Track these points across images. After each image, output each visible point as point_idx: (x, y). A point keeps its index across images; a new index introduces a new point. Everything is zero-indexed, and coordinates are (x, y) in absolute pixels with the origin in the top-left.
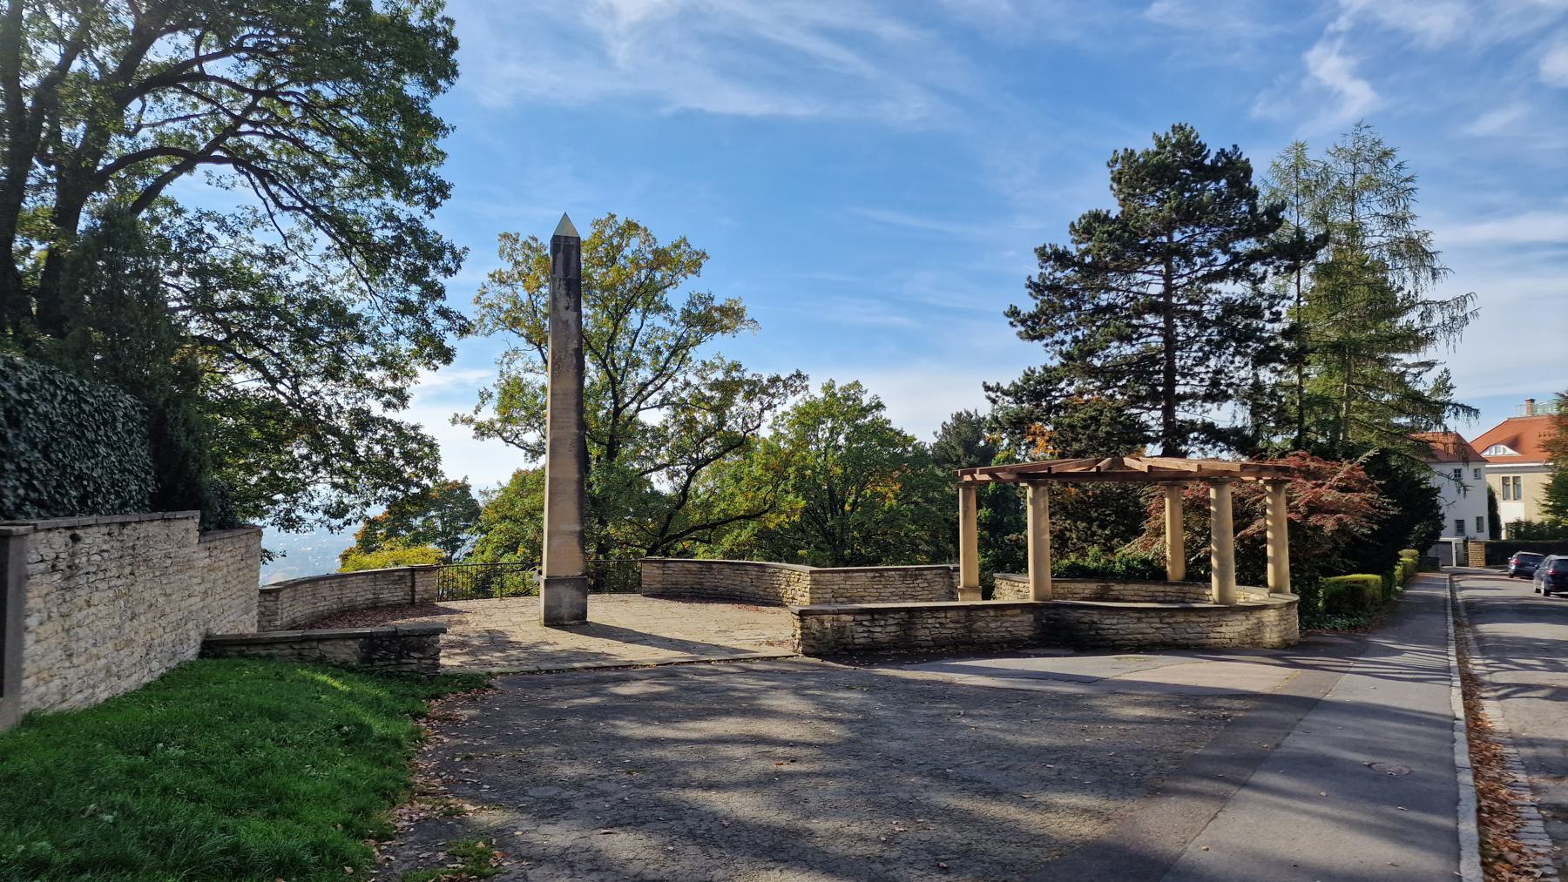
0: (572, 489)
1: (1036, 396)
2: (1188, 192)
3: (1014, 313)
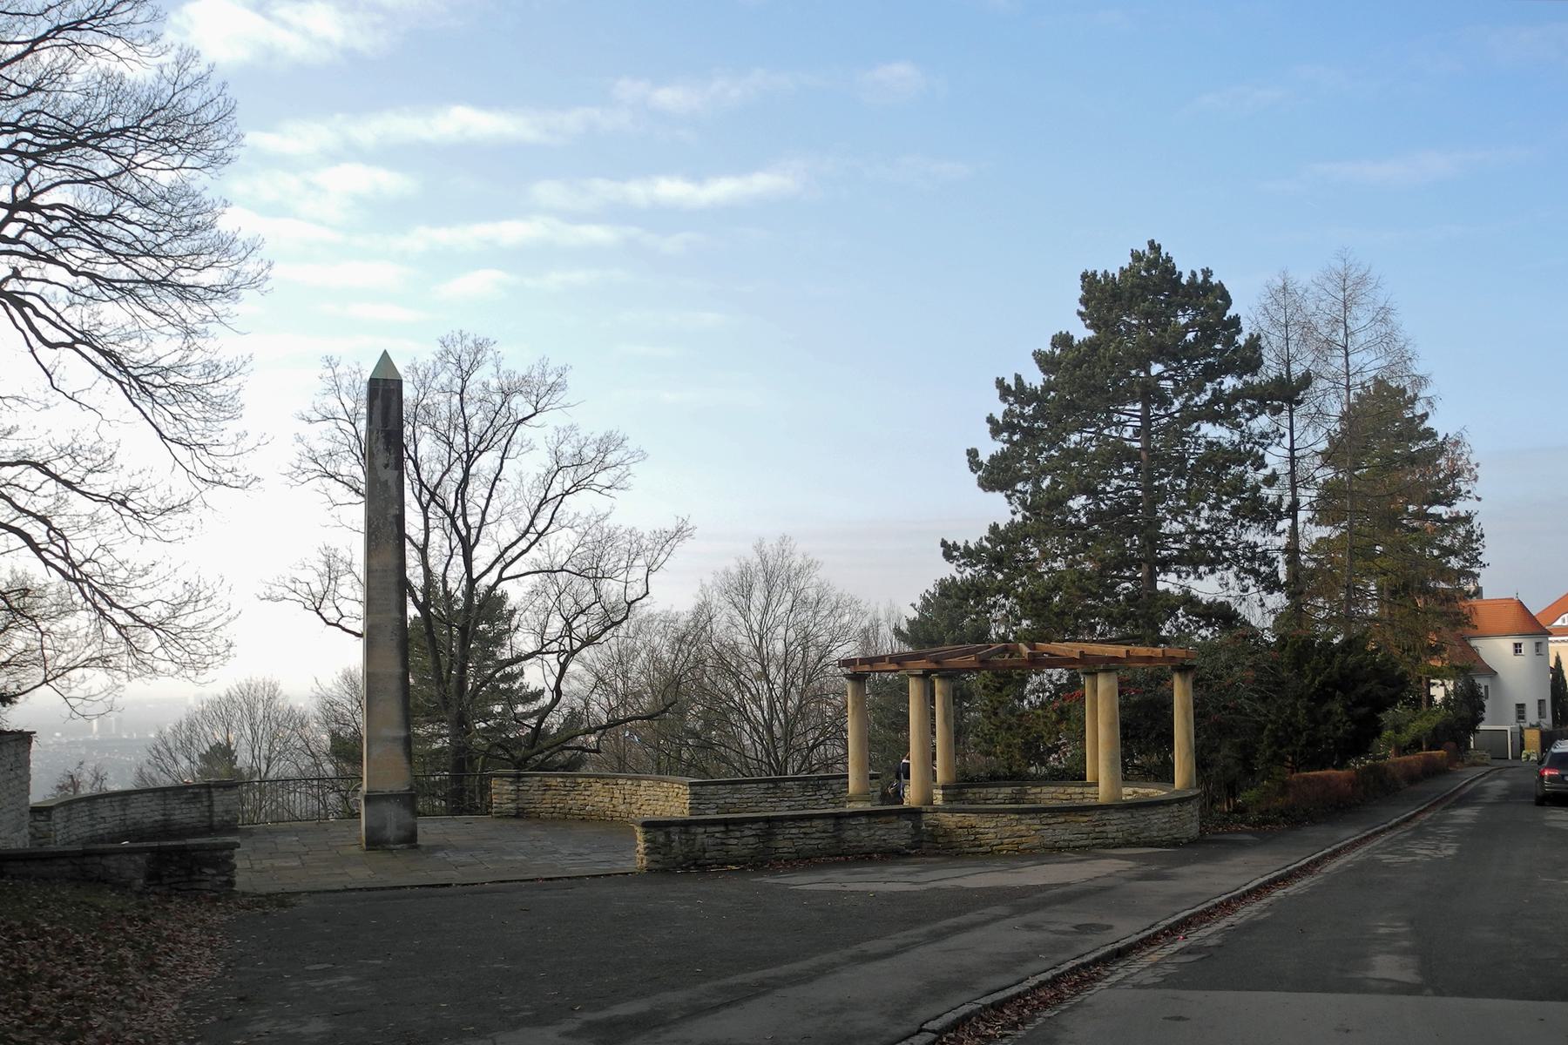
0: (394, 685)
1: (998, 561)
2: (1152, 323)
3: (973, 454)
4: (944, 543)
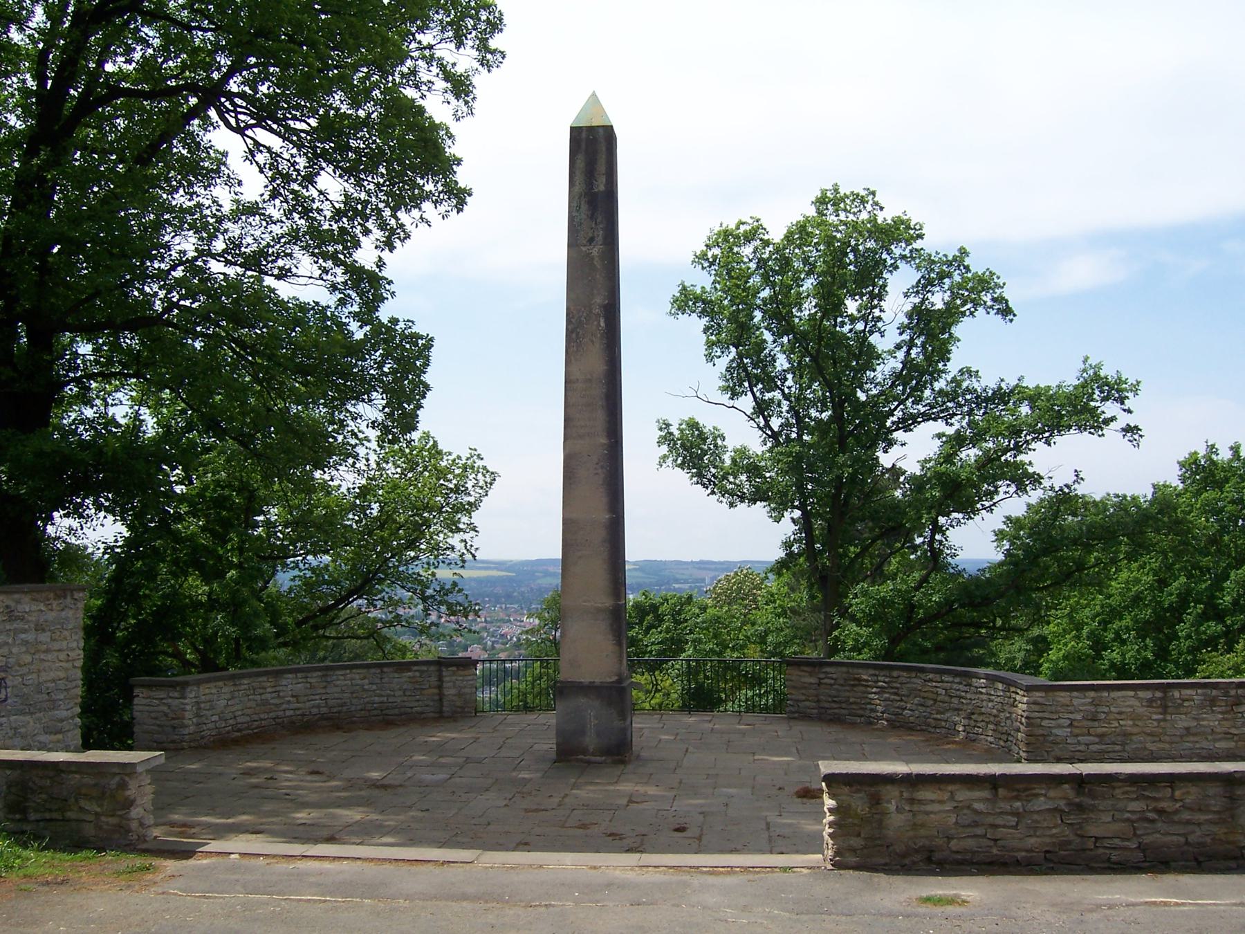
4: (594, 95)
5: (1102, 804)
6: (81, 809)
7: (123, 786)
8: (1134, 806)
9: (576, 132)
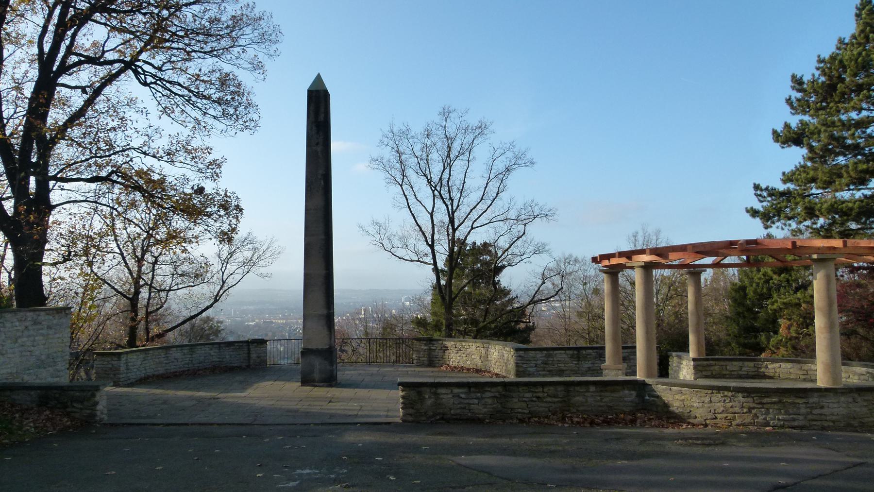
4: (319, 75)
5: (514, 395)
6: (74, 407)
7: (94, 396)
8: (527, 395)
9: (309, 91)
